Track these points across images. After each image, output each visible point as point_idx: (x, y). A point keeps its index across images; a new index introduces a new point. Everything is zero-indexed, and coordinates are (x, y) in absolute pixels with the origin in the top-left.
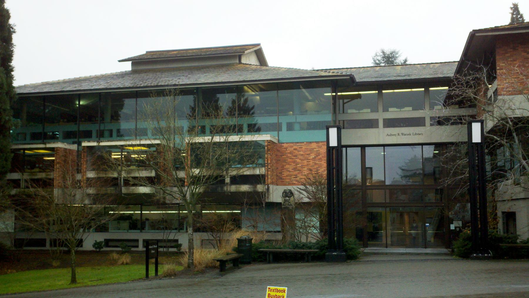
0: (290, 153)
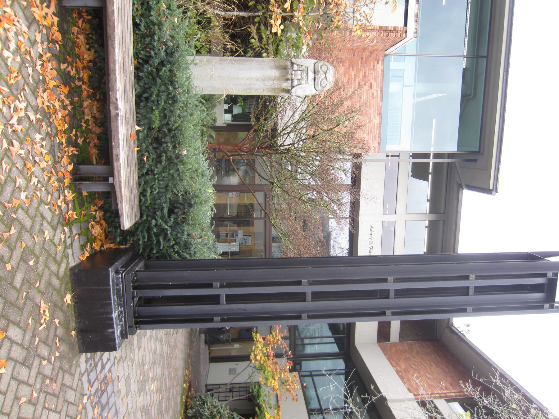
0: (365, 76)
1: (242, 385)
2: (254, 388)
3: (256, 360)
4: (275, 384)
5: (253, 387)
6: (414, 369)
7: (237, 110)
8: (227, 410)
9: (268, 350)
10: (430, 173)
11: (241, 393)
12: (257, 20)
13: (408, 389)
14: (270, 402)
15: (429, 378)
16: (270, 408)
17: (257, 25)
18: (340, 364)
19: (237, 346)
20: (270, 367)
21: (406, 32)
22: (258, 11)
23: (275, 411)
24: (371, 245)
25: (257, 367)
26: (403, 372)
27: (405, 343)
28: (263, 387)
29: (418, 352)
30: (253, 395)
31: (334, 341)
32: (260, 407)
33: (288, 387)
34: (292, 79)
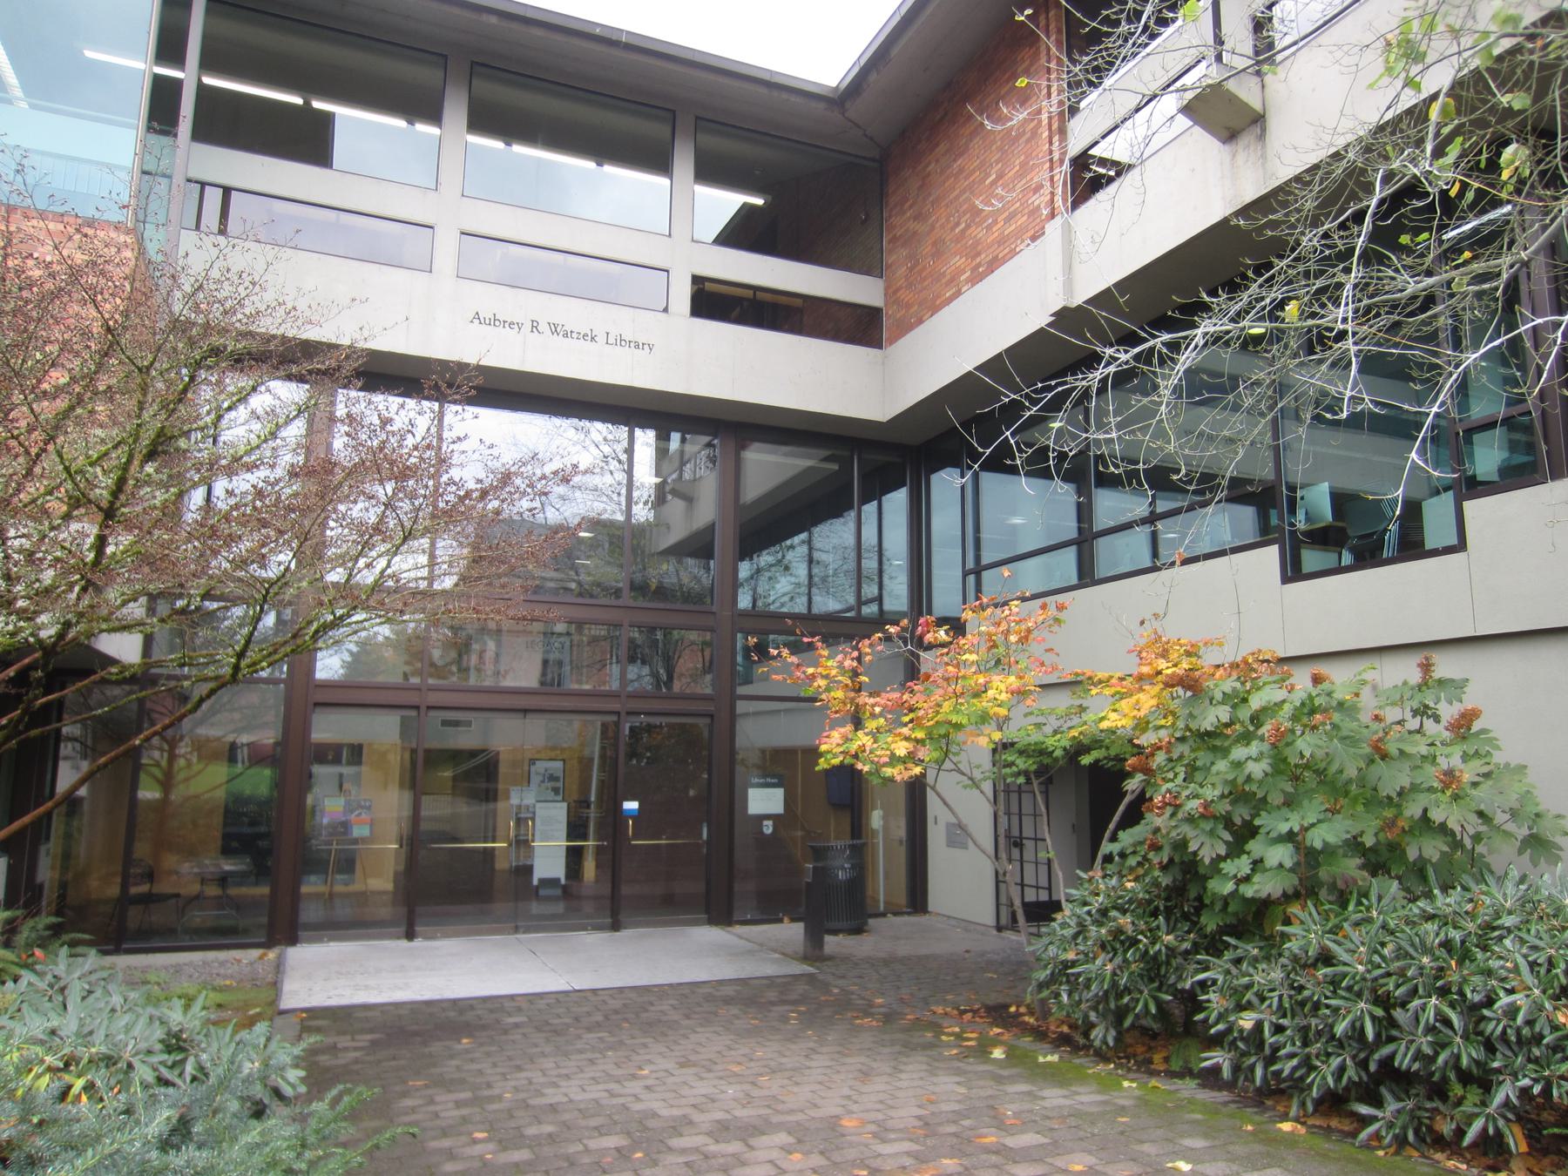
1: (1002, 807)
2: (1015, 769)
3: (911, 757)
4: (1000, 686)
5: (1007, 770)
6: (968, 227)
8: (1090, 880)
9: (877, 710)
10: (307, 103)
11: (1027, 807)
13: (1034, 238)
14: (1061, 710)
15: (1000, 176)
16: (1082, 709)
18: (947, 484)
19: (876, 819)
20: (940, 706)
23: (1094, 692)
24: (543, 327)
25: (936, 755)
26: (978, 260)
27: (889, 259)
28: (1011, 733)
29: (916, 218)
30: (1038, 773)
31: (875, 503)
32: (1080, 748)
33: (1013, 638)
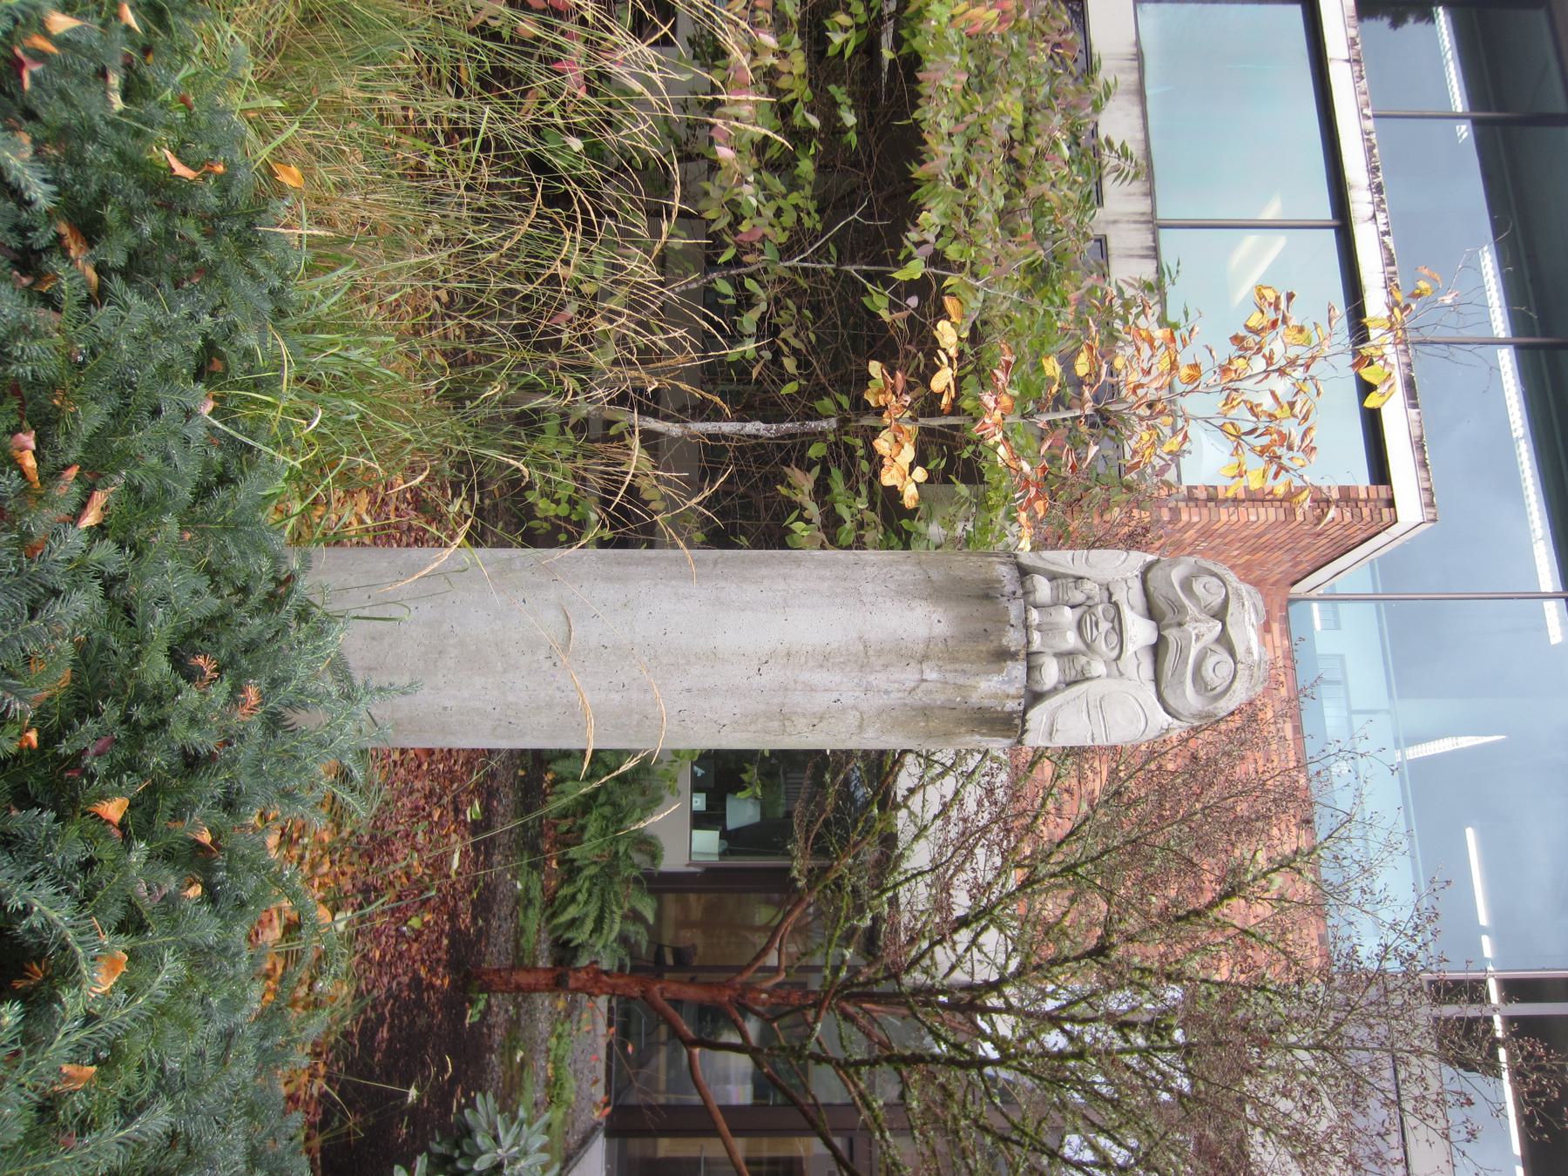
7: (742, 811)
12: (817, 450)
17: (816, 470)
21: (1391, 503)
22: (818, 417)
34: (1029, 655)
